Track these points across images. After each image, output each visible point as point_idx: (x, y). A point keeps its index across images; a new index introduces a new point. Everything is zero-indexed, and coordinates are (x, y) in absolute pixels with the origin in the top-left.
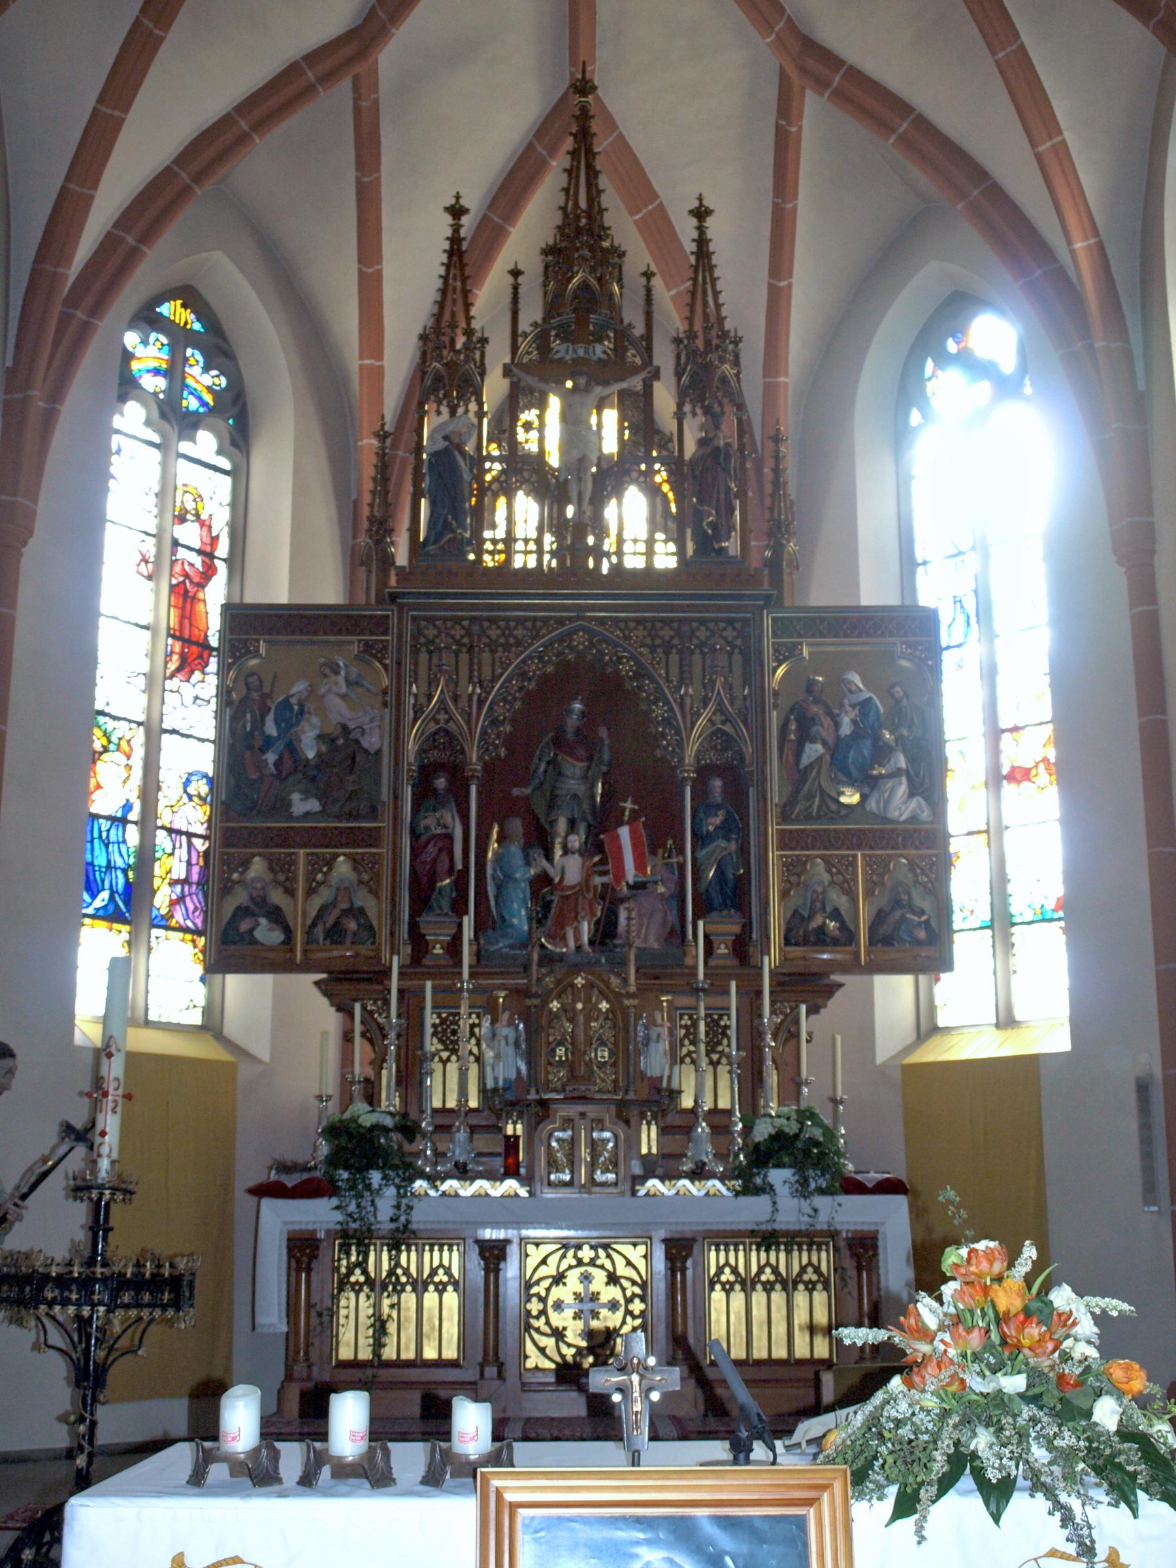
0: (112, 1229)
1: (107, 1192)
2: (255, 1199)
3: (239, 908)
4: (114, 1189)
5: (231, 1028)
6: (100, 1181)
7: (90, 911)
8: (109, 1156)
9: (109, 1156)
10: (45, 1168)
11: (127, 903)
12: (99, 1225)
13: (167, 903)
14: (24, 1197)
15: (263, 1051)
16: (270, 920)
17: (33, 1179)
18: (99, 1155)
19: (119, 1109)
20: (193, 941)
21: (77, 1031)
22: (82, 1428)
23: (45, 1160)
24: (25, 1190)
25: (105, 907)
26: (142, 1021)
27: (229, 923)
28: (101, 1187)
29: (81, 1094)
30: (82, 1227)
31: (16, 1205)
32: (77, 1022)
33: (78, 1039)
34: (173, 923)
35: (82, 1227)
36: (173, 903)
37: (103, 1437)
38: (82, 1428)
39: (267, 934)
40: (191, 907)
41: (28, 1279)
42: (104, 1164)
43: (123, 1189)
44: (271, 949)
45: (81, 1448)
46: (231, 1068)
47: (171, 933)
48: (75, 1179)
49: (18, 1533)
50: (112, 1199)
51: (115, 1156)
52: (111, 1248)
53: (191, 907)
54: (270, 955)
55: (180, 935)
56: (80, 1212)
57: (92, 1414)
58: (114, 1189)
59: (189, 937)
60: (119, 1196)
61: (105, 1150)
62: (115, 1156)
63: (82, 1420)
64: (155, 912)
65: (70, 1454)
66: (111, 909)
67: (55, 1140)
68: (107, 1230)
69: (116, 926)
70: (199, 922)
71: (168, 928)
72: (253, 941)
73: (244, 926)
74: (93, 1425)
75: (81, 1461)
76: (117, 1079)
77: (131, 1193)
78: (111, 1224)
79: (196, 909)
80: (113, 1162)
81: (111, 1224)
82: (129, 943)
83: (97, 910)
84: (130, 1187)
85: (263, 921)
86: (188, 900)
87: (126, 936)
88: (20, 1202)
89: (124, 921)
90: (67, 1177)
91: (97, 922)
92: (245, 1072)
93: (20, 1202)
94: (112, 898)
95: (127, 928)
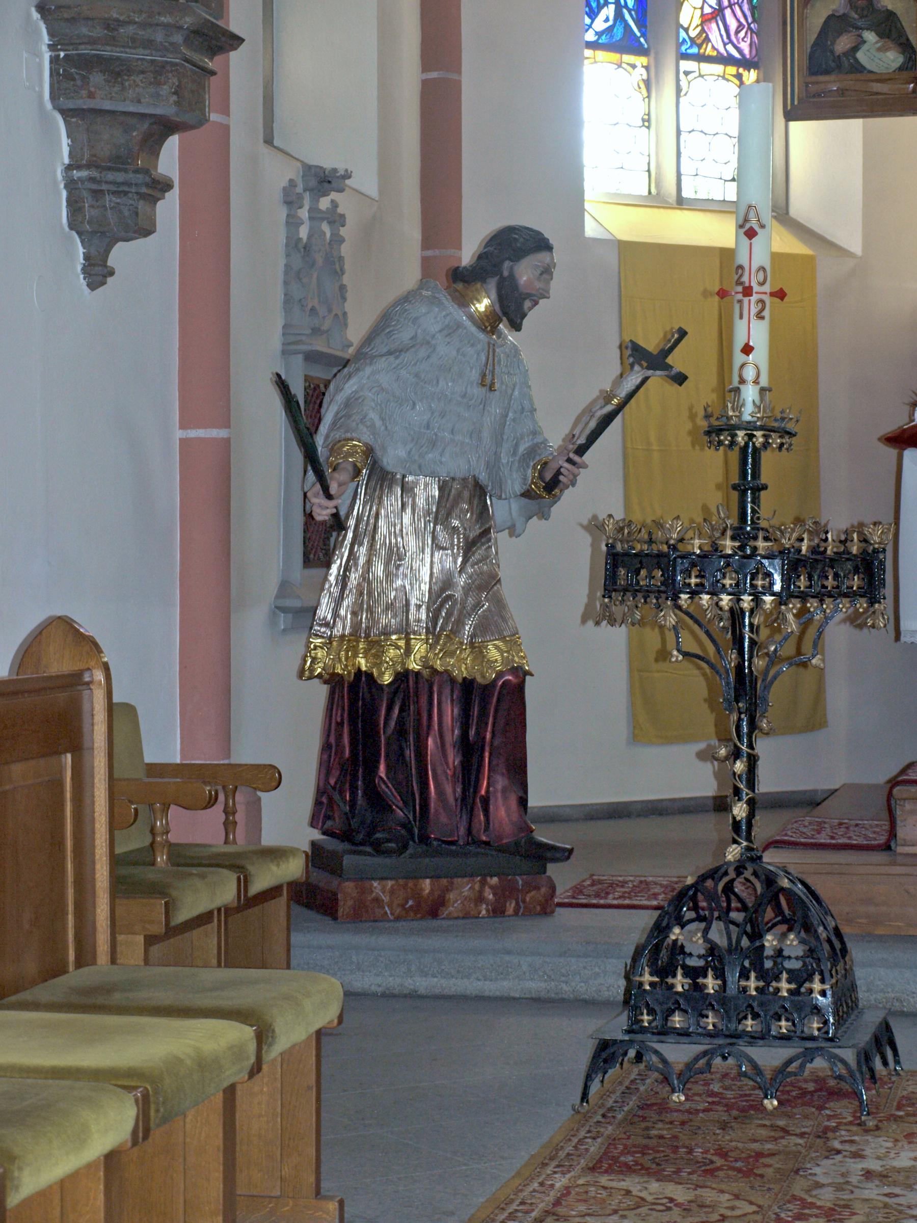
0: (765, 487)
1: (758, 434)
2: (893, 452)
3: (830, 18)
4: (768, 430)
5: (799, 207)
6: (747, 417)
7: (590, 36)
8: (756, 382)
9: (756, 382)
10: (609, 408)
11: (641, 22)
12: (747, 485)
13: (697, 21)
14: (581, 450)
15: (852, 240)
16: (881, 35)
17: (593, 424)
18: (742, 381)
19: (766, 313)
20: (739, 76)
21: (587, 218)
22: (739, 766)
23: (608, 398)
24: (582, 440)
25: (610, 30)
26: (673, 199)
27: (815, 44)
28: (750, 427)
29: (706, 294)
30: (718, 487)
31: (569, 461)
32: (587, 206)
33: (591, 230)
34: (709, 51)
35: (718, 487)
36: (706, 19)
37: (767, 784)
38: (739, 766)
39: (878, 56)
40: (733, 25)
41: (660, 560)
42: (750, 394)
43: (778, 429)
44: (882, 79)
45: (737, 792)
46: (808, 262)
47: (706, 67)
48: (707, 416)
49: (656, 913)
50: (766, 445)
51: (764, 381)
52: (764, 512)
53: (733, 25)
54: (877, 87)
55: (718, 69)
56: (715, 465)
57: (751, 746)
58: (768, 430)
59: (732, 70)
60: (775, 440)
61: (750, 374)
62: (764, 381)
63: (736, 754)
64: (683, 34)
65: (721, 805)
66: (619, 32)
67: (616, 369)
68: (758, 489)
69: (628, 58)
70: (745, 46)
71: (701, 58)
72: (858, 68)
73: (842, 44)
74: (752, 761)
75: (740, 810)
76: (762, 269)
77: (791, 434)
78: (764, 479)
79: (740, 26)
80: (763, 390)
81: (764, 479)
82: (647, 83)
83: (599, 34)
84: (790, 426)
85: (870, 37)
86: (728, 12)
87: (641, 73)
88: (576, 458)
89: (641, 51)
90: (692, 417)
91: (601, 55)
92: (828, 271)
93: (576, 458)
94: (619, 15)
95: (641, 61)
